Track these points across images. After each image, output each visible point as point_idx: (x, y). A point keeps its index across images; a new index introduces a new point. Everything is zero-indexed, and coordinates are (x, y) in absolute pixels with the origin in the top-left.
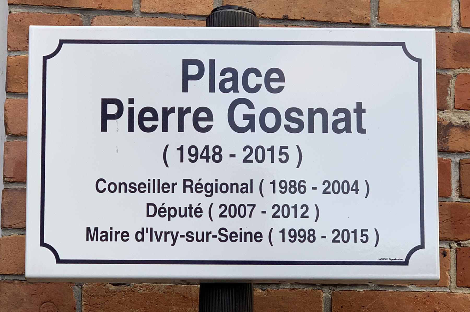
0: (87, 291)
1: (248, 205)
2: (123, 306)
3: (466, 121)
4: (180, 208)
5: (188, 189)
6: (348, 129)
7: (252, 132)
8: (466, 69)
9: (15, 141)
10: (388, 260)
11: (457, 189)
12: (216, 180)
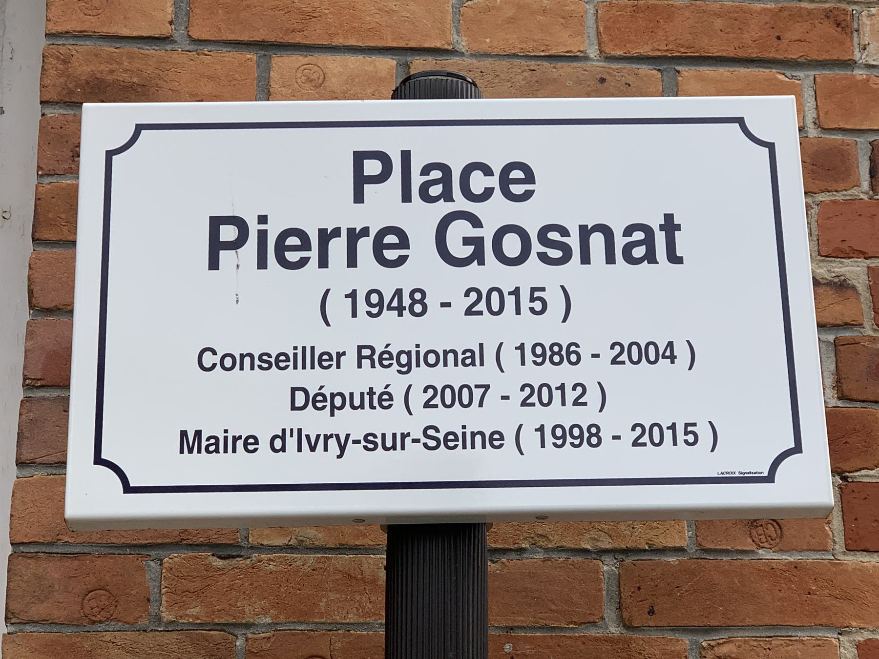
0: (171, 569)
1: (477, 386)
2: (237, 594)
3: (841, 276)
5: (366, 363)
6: (650, 257)
7: (479, 264)
8: (834, 193)
9: (46, 318)
10: (737, 475)
11: (834, 387)
12: (418, 346)
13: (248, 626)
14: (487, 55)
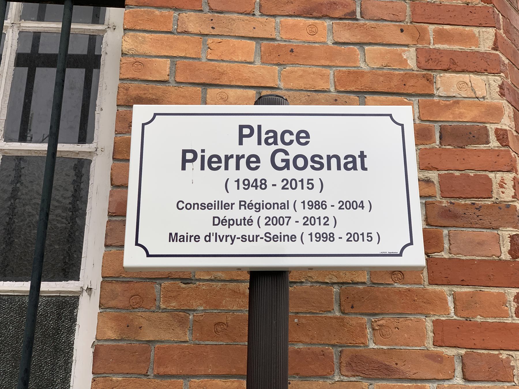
1: (286, 217)
4: (237, 220)
5: (243, 207)
6: (355, 168)
10: (388, 253)
12: (263, 201)
13: (194, 310)
14: (291, 90)
